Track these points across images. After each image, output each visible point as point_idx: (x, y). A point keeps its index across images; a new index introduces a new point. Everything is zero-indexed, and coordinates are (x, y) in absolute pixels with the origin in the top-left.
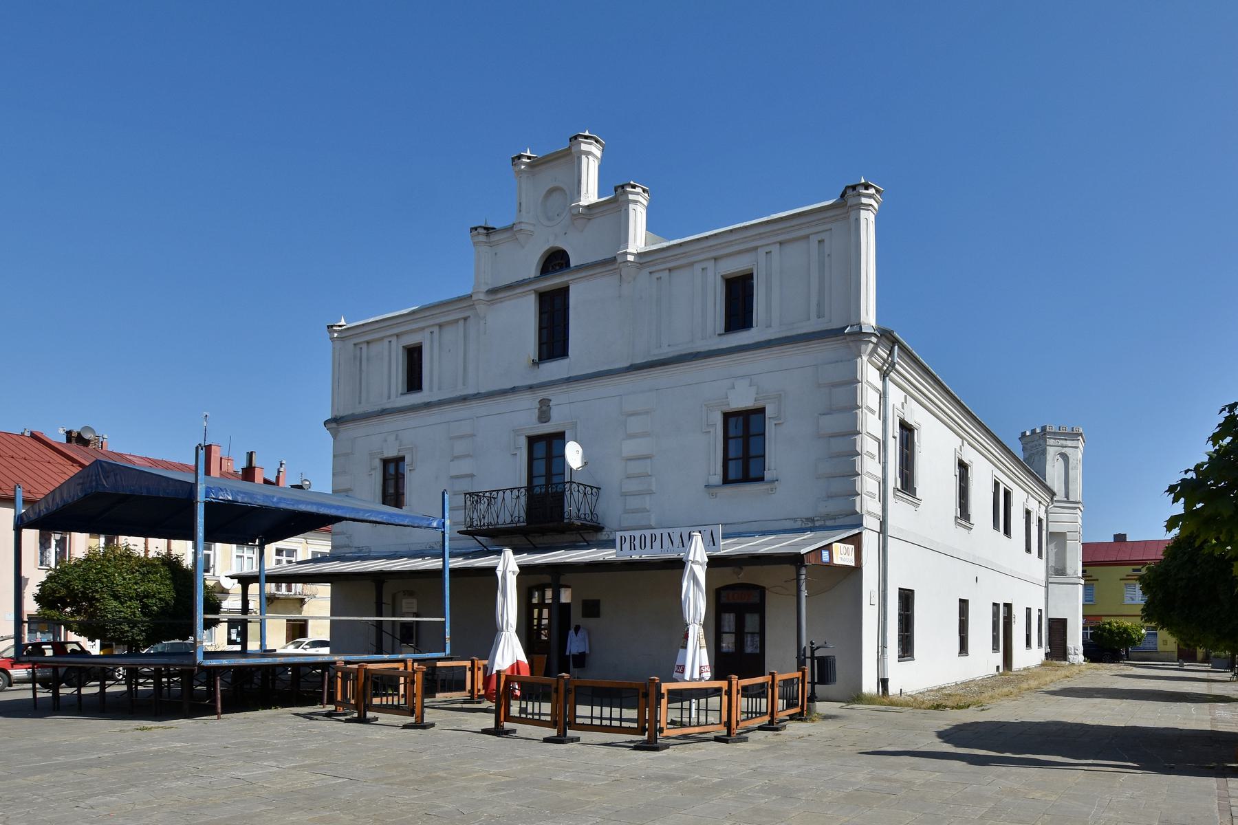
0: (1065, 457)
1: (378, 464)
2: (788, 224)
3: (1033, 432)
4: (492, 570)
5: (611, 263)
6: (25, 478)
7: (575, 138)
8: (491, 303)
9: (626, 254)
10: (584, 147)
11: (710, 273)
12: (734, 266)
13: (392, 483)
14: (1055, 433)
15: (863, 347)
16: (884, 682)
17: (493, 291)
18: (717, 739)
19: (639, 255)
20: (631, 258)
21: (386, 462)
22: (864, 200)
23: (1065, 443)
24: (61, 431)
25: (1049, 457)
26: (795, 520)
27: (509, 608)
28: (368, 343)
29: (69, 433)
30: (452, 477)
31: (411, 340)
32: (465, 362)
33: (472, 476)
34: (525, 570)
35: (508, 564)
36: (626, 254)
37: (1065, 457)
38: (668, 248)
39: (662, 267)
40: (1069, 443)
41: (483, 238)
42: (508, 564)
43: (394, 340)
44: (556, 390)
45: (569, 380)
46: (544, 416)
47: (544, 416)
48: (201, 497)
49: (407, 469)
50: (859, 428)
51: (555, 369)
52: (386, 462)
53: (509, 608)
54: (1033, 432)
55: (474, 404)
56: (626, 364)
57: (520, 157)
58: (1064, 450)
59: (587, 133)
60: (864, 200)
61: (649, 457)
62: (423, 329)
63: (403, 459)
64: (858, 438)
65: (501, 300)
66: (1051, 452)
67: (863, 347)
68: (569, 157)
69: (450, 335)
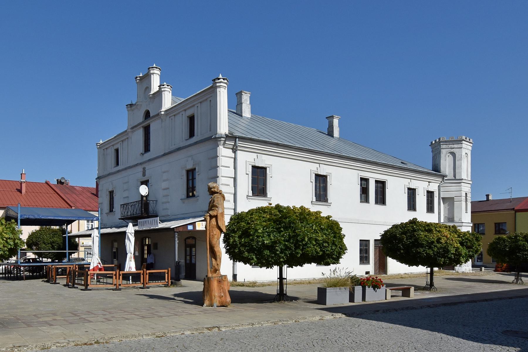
0: (453, 154)
1: (184, 173)
2: (207, 92)
3: (435, 141)
4: (124, 233)
5: (158, 115)
6: (47, 198)
7: (149, 68)
8: (133, 132)
9: (161, 112)
10: (152, 72)
11: (184, 115)
12: (189, 113)
13: (191, 182)
14: (446, 141)
15: (219, 142)
16: (235, 276)
17: (132, 128)
18: (140, 288)
19: (166, 111)
20: (163, 113)
21: (188, 172)
22: (218, 85)
23: (452, 146)
24: (55, 180)
25: (442, 156)
26: (202, 212)
27: (130, 245)
28: (106, 149)
29: (58, 180)
30: (124, 198)
31: (115, 147)
32: (211, 120)
33: (128, 197)
34: (136, 232)
35: (130, 229)
36: (161, 112)
37: (453, 154)
38: (175, 106)
39: (172, 115)
40: (455, 146)
41: (129, 109)
42: (130, 229)
43: (184, 113)
44: (147, 164)
45: (150, 160)
46: (144, 175)
47: (144, 175)
48: (19, 218)
49: (197, 174)
50: (218, 175)
51: (148, 156)
52: (188, 172)
53: (130, 245)
54: (435, 141)
55: (123, 172)
56: (163, 153)
57: (137, 77)
58: (452, 150)
59: (154, 66)
60: (218, 85)
61: (168, 188)
62: (118, 143)
63: (195, 169)
64: (218, 179)
65: (135, 131)
66: (444, 152)
67: (219, 142)
68: (147, 77)
69: (125, 143)
